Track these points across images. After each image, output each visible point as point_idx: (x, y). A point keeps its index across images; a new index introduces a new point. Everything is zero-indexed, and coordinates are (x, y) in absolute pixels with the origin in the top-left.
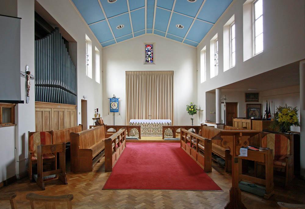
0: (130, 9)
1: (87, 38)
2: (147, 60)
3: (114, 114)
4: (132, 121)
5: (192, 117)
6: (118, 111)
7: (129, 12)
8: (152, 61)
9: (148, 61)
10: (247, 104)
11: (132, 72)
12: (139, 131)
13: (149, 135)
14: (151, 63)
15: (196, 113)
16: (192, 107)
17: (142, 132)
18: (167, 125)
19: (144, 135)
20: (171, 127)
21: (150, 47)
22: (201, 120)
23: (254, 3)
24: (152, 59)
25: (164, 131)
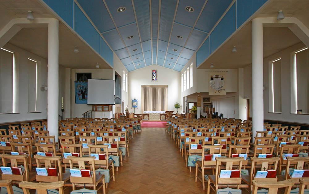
0: (142, 41)
1: (124, 71)
4: (145, 112)
7: (144, 60)
9: (154, 79)
10: (204, 103)
12: (149, 117)
15: (179, 108)
17: (150, 118)
18: (163, 114)
25: (160, 117)
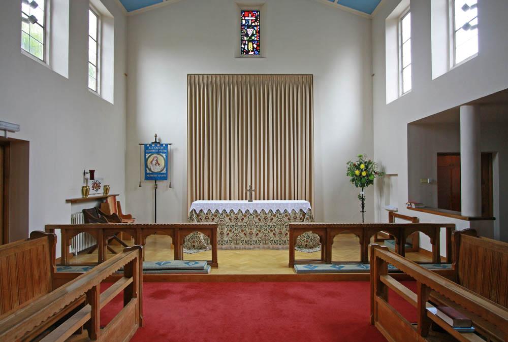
2: (244, 49)
3: (156, 185)
4: (198, 204)
5: (363, 193)
6: (165, 178)
8: (257, 50)
9: (248, 52)
11: (205, 76)
12: (213, 243)
13: (247, 246)
14: (255, 56)
15: (371, 182)
16: (362, 166)
19: (233, 246)
20: (315, 229)
21: (252, 17)
22: (394, 201)
23: (402, 19)
24: (258, 45)
